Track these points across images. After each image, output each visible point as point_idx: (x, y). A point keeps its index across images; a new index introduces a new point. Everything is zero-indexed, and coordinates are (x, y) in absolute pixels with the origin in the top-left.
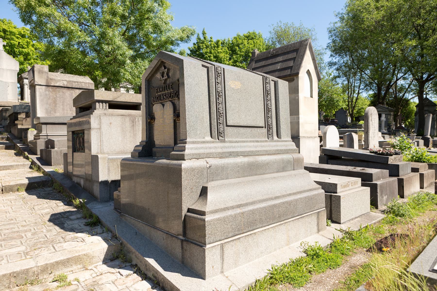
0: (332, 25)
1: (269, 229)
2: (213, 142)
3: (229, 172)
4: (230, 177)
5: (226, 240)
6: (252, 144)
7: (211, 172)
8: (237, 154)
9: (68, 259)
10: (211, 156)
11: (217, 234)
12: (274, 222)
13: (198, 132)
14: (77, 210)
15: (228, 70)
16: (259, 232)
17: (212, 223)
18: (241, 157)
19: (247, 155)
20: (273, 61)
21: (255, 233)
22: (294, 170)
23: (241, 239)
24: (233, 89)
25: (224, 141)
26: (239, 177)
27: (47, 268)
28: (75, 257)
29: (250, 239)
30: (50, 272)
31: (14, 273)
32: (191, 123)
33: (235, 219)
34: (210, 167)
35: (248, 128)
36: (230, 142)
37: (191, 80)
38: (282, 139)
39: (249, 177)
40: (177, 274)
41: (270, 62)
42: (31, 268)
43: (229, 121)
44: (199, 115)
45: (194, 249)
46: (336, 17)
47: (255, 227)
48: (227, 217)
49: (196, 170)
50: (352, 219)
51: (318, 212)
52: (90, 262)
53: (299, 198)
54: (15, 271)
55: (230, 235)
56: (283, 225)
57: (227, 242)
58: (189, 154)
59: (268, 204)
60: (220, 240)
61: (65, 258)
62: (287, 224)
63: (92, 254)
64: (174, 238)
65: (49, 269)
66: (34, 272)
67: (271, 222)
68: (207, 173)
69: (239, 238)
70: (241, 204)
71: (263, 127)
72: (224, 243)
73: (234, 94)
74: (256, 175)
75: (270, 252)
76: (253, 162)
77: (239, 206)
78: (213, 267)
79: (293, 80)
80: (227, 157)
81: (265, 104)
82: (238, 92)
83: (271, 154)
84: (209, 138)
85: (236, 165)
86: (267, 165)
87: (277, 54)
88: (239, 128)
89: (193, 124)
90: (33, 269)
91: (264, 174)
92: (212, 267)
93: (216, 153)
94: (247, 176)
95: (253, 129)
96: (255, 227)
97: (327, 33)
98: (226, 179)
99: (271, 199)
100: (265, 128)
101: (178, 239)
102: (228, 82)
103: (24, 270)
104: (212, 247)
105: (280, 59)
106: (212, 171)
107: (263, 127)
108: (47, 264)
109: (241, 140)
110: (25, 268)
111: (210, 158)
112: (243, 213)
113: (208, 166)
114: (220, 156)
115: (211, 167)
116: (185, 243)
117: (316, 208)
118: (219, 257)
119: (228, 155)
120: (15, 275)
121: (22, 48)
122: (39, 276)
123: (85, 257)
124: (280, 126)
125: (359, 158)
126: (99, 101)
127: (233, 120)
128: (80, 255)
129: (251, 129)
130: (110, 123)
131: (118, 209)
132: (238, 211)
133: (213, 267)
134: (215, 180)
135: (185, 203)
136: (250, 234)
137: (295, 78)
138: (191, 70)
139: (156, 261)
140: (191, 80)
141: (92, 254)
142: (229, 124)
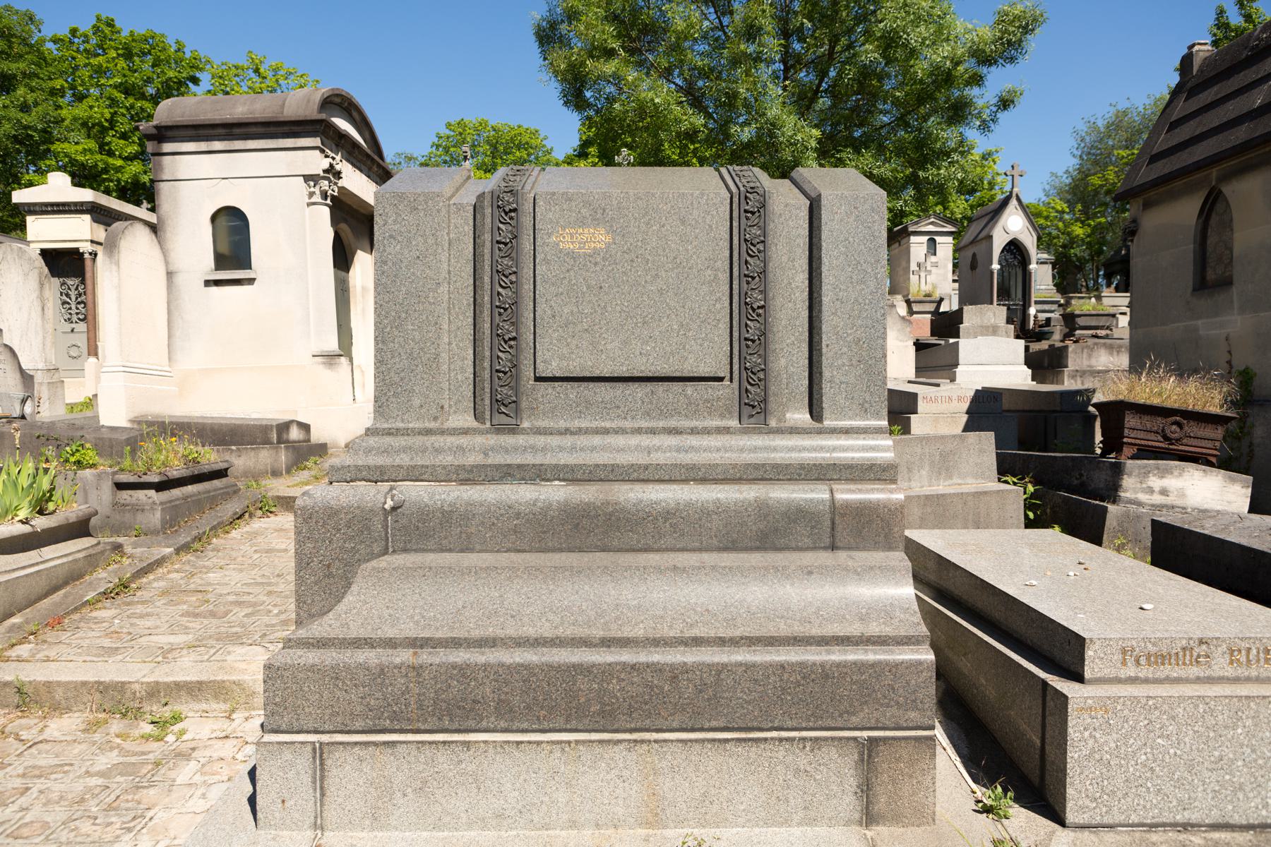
1: (539, 743)
2: (481, 432)
3: (473, 530)
4: (478, 547)
5: (339, 735)
6: (634, 440)
7: (398, 525)
8: (539, 474)
9: (200, 683)
10: (425, 477)
11: (307, 710)
12: (573, 724)
13: (416, 402)
15: (554, 194)
16: (485, 742)
17: (286, 674)
18: (557, 483)
19: (586, 477)
21: (467, 744)
22: (833, 547)
23: (400, 748)
24: (571, 255)
25: (513, 430)
26: (519, 551)
27: (159, 692)
28: (214, 681)
29: (442, 757)
30: (163, 701)
31: (99, 683)
32: (392, 374)
33: (379, 680)
34: (394, 509)
35: (636, 385)
36: (539, 432)
37: (398, 247)
38: (827, 423)
39: (564, 556)
42: (130, 682)
43: (544, 362)
44: (422, 349)
47: (472, 724)
48: (347, 668)
49: (343, 516)
50: (1186, 827)
51: (872, 740)
52: (248, 703)
53: (740, 664)
54: (102, 680)
55: (359, 725)
56: (621, 747)
57: (341, 743)
58: (343, 467)
59: (544, 659)
60: (316, 732)
61: (195, 679)
62: (645, 747)
63: (251, 684)
65: (162, 694)
66: (134, 693)
67: (561, 722)
68: (386, 527)
69: (394, 743)
70: (428, 639)
71: (721, 379)
72: (328, 744)
73: (572, 273)
74: (604, 549)
75: (546, 827)
76: (588, 504)
77: (416, 643)
78: (283, 801)
80: (492, 481)
81: (736, 292)
82: (596, 264)
83: (716, 481)
84: (469, 421)
85: (511, 511)
86: (666, 520)
88: (591, 385)
89: (396, 379)
90: (133, 686)
91: (647, 549)
92: (280, 801)
93: (444, 467)
94: (561, 550)
95: (660, 388)
96: (472, 724)
97: (202, 54)
98: (462, 551)
99: (585, 643)
100: (731, 381)
102: (550, 235)
103: (118, 683)
104: (279, 743)
106: (404, 521)
107: (721, 379)
108: (157, 683)
109: (594, 424)
110: (120, 680)
111: (422, 481)
112: (418, 669)
113: (387, 506)
114: (461, 477)
115: (399, 511)
117: (855, 720)
118: (307, 779)
119: (497, 475)
120: (103, 688)
122: (144, 704)
123: (235, 687)
124: (821, 373)
127: (562, 358)
128: (224, 681)
129: (649, 386)
132: (404, 656)
133: (283, 801)
134: (416, 551)
135: (305, 603)
136: (444, 743)
138: (399, 219)
140: (398, 247)
141: (251, 684)
142: (543, 371)
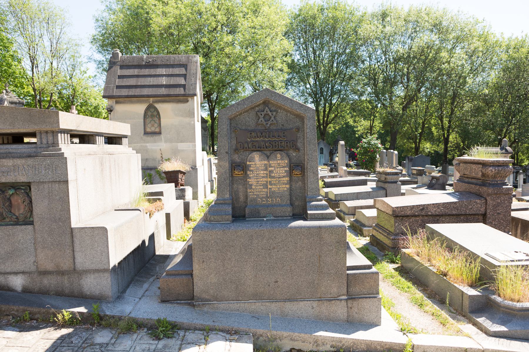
0: (100, 13)
14: (73, 329)
20: (152, 71)
40: (220, 342)
41: (146, 72)
45: (366, 303)
46: (101, 3)
64: (333, 302)
79: (188, 101)
87: (155, 63)
101: (341, 300)
105: (163, 71)
116: (350, 302)
121: (120, 52)
125: (210, 172)
126: (64, 131)
130: (85, 169)
131: (340, 296)
137: (190, 99)
139: (323, 331)
